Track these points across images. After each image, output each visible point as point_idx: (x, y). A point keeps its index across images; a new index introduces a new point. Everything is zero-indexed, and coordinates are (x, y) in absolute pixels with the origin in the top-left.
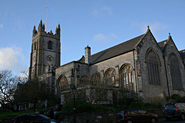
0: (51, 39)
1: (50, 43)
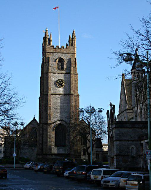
0: (60, 56)
1: (61, 60)
